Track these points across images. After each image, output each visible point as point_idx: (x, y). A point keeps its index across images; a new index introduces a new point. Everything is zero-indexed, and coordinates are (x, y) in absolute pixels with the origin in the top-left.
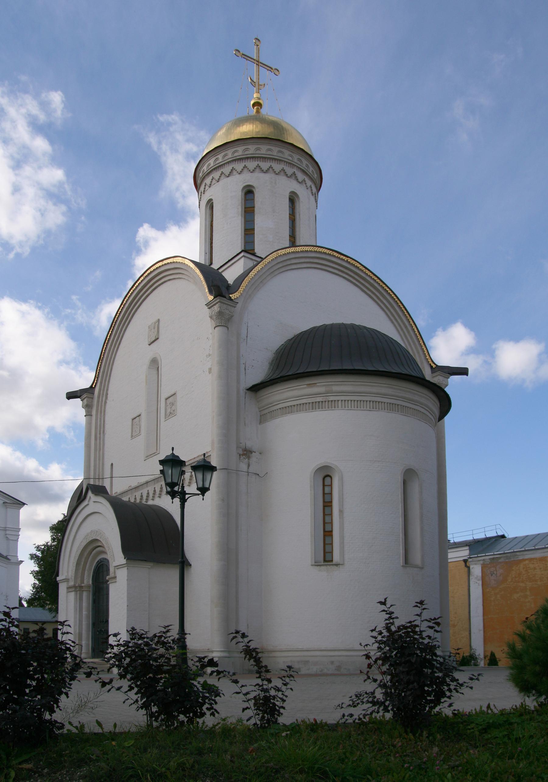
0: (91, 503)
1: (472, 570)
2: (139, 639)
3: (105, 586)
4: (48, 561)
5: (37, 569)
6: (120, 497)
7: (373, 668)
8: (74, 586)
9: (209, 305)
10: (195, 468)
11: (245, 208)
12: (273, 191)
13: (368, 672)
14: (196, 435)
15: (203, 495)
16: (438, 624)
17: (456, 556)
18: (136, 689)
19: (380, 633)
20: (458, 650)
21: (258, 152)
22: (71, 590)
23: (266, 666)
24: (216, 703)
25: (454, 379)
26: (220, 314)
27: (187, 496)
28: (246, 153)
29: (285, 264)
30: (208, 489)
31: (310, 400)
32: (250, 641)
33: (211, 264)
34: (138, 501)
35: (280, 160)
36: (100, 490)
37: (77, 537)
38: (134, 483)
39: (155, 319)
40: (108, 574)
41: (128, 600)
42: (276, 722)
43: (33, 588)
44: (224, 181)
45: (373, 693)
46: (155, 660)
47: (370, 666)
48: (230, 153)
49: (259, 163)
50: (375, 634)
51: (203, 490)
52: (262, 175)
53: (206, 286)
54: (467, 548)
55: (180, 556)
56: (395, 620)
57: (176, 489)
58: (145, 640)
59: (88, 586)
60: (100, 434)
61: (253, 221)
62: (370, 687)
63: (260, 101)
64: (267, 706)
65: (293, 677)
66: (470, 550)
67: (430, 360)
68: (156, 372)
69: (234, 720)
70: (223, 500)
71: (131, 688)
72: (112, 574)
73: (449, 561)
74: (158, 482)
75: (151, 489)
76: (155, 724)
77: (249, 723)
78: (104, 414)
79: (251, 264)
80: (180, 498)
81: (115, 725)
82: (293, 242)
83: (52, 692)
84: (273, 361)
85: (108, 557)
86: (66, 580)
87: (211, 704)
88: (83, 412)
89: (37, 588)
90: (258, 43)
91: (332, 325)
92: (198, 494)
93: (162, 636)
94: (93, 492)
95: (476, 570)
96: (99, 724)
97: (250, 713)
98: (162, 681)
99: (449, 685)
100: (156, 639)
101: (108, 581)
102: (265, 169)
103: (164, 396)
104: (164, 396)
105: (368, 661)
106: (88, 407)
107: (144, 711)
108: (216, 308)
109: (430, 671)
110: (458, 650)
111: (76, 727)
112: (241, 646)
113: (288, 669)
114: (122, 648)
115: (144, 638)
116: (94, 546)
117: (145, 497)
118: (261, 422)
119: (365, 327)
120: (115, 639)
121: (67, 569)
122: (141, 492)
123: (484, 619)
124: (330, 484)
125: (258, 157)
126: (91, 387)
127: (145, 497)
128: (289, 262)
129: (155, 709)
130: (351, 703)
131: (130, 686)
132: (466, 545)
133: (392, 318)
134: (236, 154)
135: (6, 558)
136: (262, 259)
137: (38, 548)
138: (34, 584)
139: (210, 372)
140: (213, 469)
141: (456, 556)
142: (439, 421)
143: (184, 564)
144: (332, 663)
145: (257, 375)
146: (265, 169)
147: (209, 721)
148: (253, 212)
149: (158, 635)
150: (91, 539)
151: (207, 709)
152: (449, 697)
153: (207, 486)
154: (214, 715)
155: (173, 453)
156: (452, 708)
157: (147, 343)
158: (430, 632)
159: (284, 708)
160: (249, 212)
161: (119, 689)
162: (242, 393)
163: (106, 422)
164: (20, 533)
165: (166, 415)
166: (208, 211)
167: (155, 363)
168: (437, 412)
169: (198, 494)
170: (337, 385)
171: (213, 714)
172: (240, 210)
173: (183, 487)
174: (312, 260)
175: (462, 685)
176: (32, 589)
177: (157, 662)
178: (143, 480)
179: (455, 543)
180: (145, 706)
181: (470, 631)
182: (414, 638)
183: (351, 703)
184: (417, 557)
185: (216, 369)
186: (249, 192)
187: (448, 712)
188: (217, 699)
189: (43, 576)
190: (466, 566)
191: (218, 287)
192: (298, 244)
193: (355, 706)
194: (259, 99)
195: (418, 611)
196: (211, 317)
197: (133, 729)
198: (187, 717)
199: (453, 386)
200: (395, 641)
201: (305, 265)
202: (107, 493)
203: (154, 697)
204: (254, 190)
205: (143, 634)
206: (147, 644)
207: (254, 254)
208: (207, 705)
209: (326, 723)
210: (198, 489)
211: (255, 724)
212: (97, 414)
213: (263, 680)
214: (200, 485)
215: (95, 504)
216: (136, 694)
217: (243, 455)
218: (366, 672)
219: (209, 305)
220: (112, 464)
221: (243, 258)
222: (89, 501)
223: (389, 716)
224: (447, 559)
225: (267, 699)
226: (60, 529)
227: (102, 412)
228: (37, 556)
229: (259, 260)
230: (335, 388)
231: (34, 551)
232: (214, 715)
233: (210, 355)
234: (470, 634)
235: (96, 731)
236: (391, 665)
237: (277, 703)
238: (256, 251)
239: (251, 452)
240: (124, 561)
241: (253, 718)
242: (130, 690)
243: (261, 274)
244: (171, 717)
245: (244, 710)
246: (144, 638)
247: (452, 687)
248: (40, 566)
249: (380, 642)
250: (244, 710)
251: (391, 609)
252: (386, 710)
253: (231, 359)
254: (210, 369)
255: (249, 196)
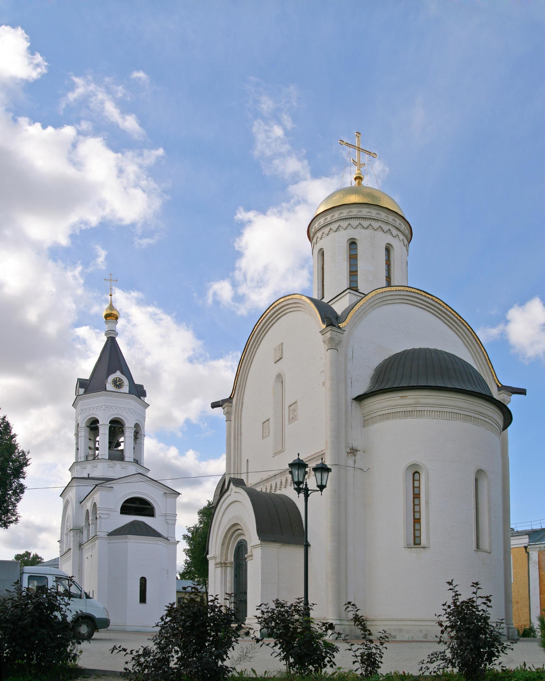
0: (233, 493)
1: (531, 556)
2: (281, 608)
3: (244, 562)
4: (199, 541)
5: (188, 547)
6: (254, 488)
7: (445, 633)
8: (221, 563)
9: (322, 332)
10: (315, 469)
11: (350, 272)
12: (372, 243)
13: (441, 637)
14: (313, 440)
15: (322, 491)
16: (490, 601)
17: (518, 543)
18: (279, 645)
19: (449, 607)
20: (502, 620)
21: (360, 214)
22: (217, 566)
23: (369, 631)
24: (334, 657)
25: (515, 397)
26: (331, 339)
27: (309, 492)
28: (350, 214)
29: (382, 300)
30: (325, 486)
31: (403, 410)
32: (358, 610)
33: (323, 298)
34: (268, 491)
35: (378, 220)
36: (239, 483)
37: (222, 522)
38: (265, 476)
39: (280, 343)
40: (246, 553)
41: (262, 575)
42: (376, 673)
43: (185, 563)
44: (332, 234)
45: (444, 652)
46: (293, 624)
47: (442, 632)
48: (336, 215)
49: (360, 221)
50: (445, 607)
51: (322, 487)
52: (364, 230)
53: (320, 319)
54: (527, 536)
55: (305, 541)
56: (459, 596)
57: (301, 486)
58: (286, 608)
59: (231, 563)
60: (238, 435)
61: (357, 265)
62: (442, 647)
63: (361, 176)
64: (370, 661)
65: (387, 638)
66: (529, 538)
67: (497, 381)
68: (281, 385)
69: (347, 670)
70: (335, 491)
71: (276, 644)
72: (249, 553)
73: (512, 547)
74: (284, 475)
75: (278, 481)
76: (292, 672)
77: (357, 672)
78: (241, 420)
79: (355, 299)
80: (304, 494)
81: (266, 672)
82: (389, 284)
83: (223, 645)
84: (373, 376)
85: (246, 538)
86: (214, 558)
87: (330, 658)
88: (224, 417)
89: (188, 564)
90: (358, 135)
91: (420, 349)
92: (318, 491)
93: (297, 605)
94: (234, 485)
95: (534, 555)
96: (254, 671)
97: (357, 665)
98: (297, 640)
99: (497, 648)
100: (293, 608)
101: (246, 559)
102: (365, 226)
103: (287, 403)
104: (287, 403)
105: (441, 629)
106: (228, 414)
107: (284, 662)
108: (328, 335)
109: (484, 636)
110: (502, 620)
111: (238, 673)
112: (351, 615)
113: (383, 632)
114: (270, 614)
115: (285, 607)
116: (235, 528)
117: (273, 488)
118: (364, 426)
119: (445, 352)
120: (265, 607)
121: (214, 549)
122: (270, 483)
123: (540, 598)
124: (418, 486)
125: (360, 218)
126: (230, 397)
127: (273, 488)
128: (385, 299)
129: (292, 660)
130: (429, 660)
131: (275, 643)
132: (527, 534)
133: (468, 345)
134: (342, 215)
135: (167, 539)
136: (366, 295)
137: (189, 529)
138: (186, 560)
139: (323, 385)
140: (328, 470)
141: (518, 543)
142: (503, 430)
143: (307, 546)
144: (421, 631)
145: (362, 388)
146: (365, 226)
147: (328, 670)
148: (356, 258)
149: (294, 604)
150: (233, 523)
151: (328, 661)
152: (498, 657)
153: (324, 484)
154: (332, 667)
155: (299, 458)
156: (501, 665)
157: (273, 361)
158: (484, 607)
159: (382, 663)
160: (353, 258)
161: (268, 645)
162: (349, 401)
163: (242, 426)
164: (177, 518)
165: (289, 419)
166: (320, 258)
167: (280, 378)
168: (501, 423)
169: (318, 491)
170: (423, 398)
171: (331, 666)
172: (346, 257)
173: (306, 485)
174: (404, 297)
175: (505, 648)
176: (184, 564)
177: (293, 625)
178: (272, 473)
179: (518, 532)
180: (286, 658)
181: (530, 607)
182: (473, 611)
183: (429, 660)
184: (485, 544)
185: (328, 383)
186: (353, 243)
187: (498, 668)
188: (335, 654)
189: (193, 553)
190: (526, 552)
191: (331, 319)
192: (392, 285)
193: (432, 663)
194: (360, 174)
195: (474, 590)
196: (324, 342)
197: (278, 676)
198: (314, 667)
199: (514, 403)
200: (459, 613)
201: (399, 301)
202: (244, 484)
203: (292, 651)
204: (356, 241)
205: (284, 604)
206: (287, 612)
207: (357, 291)
208: (327, 659)
209: (411, 675)
210: (318, 486)
211: (362, 674)
212: (235, 420)
213: (367, 641)
214: (319, 484)
215: (236, 494)
216: (279, 649)
217: (350, 453)
218: (439, 637)
219: (322, 332)
220: (248, 460)
221: (349, 294)
222: (231, 492)
223: (456, 670)
224: (510, 545)
225: (370, 655)
226: (208, 513)
227: (239, 417)
228: (188, 537)
229: (363, 296)
230: (422, 401)
231: (186, 533)
232: (332, 667)
233: (323, 371)
234: (530, 610)
235: (251, 676)
236: (457, 631)
237: (377, 659)
238: (359, 288)
239: (357, 451)
240: (259, 542)
241: (360, 670)
242: (275, 646)
243: (363, 308)
244: (303, 667)
245: (354, 662)
246: (285, 607)
247: (500, 649)
248: (190, 545)
249: (450, 614)
250: (354, 662)
251: (456, 589)
252: (454, 666)
253: (340, 375)
254: (324, 384)
255: (353, 246)
